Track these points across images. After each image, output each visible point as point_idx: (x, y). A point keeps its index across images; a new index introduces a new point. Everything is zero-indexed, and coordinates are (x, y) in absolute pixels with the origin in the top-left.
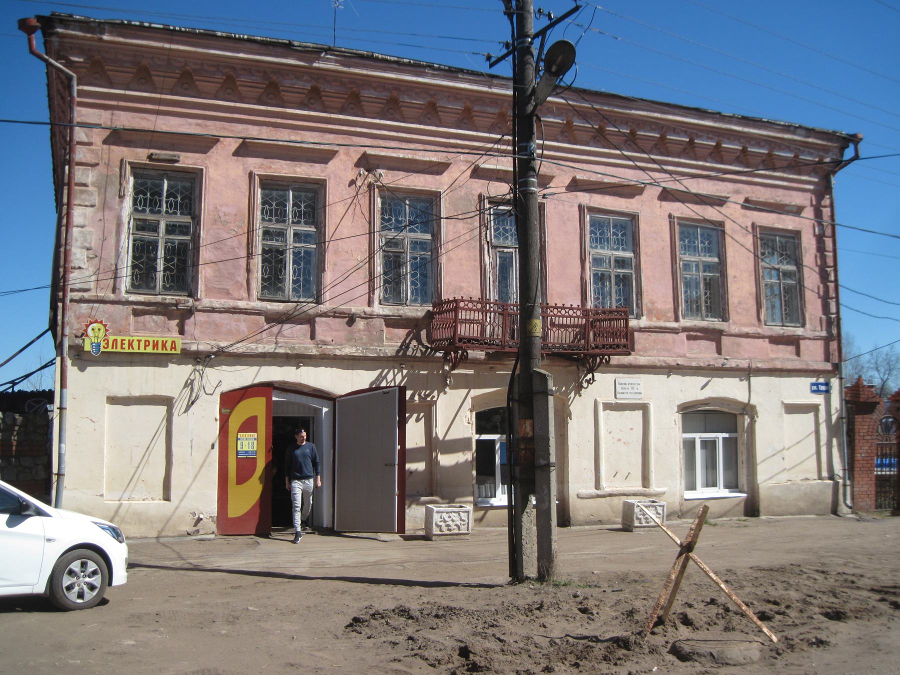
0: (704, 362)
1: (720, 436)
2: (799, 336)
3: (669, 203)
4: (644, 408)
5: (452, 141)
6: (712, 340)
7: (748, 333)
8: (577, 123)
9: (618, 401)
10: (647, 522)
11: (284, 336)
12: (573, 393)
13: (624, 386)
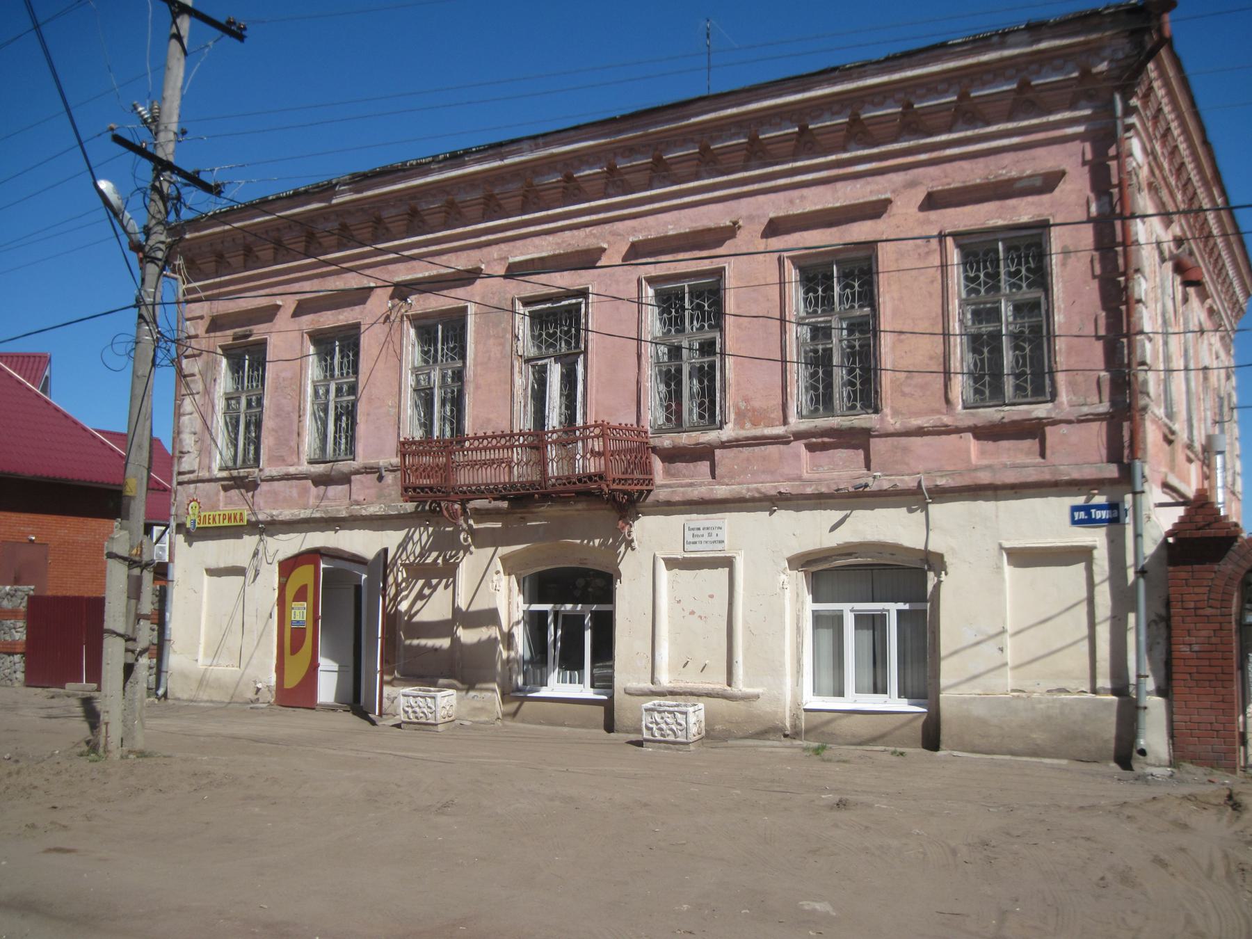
0: (828, 487)
1: (892, 609)
2: (1041, 419)
3: (780, 237)
4: (728, 563)
5: (483, 239)
6: (855, 447)
7: (921, 428)
8: (622, 164)
9: (686, 555)
10: (662, 735)
11: (329, 499)
12: (623, 546)
13: (696, 532)
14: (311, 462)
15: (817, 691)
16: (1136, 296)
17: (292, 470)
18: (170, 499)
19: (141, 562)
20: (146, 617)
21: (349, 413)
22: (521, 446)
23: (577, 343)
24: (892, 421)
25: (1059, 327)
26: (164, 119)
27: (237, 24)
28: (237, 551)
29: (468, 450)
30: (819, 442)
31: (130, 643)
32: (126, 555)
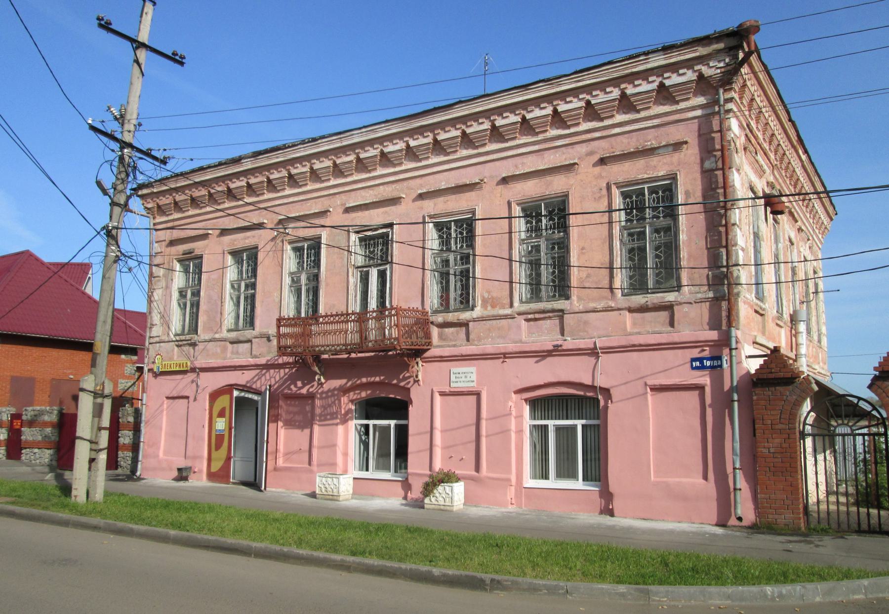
4: (478, 395)
13: (457, 375)
14: (229, 331)
15: (534, 477)
16: (732, 221)
17: (217, 336)
18: (144, 354)
19: (103, 394)
20: (105, 429)
21: (251, 300)
22: (353, 321)
23: (387, 257)
24: (577, 305)
25: (683, 243)
26: (128, 117)
27: (179, 55)
28: (181, 385)
29: (321, 323)
30: (533, 318)
31: (93, 445)
32: (92, 390)
